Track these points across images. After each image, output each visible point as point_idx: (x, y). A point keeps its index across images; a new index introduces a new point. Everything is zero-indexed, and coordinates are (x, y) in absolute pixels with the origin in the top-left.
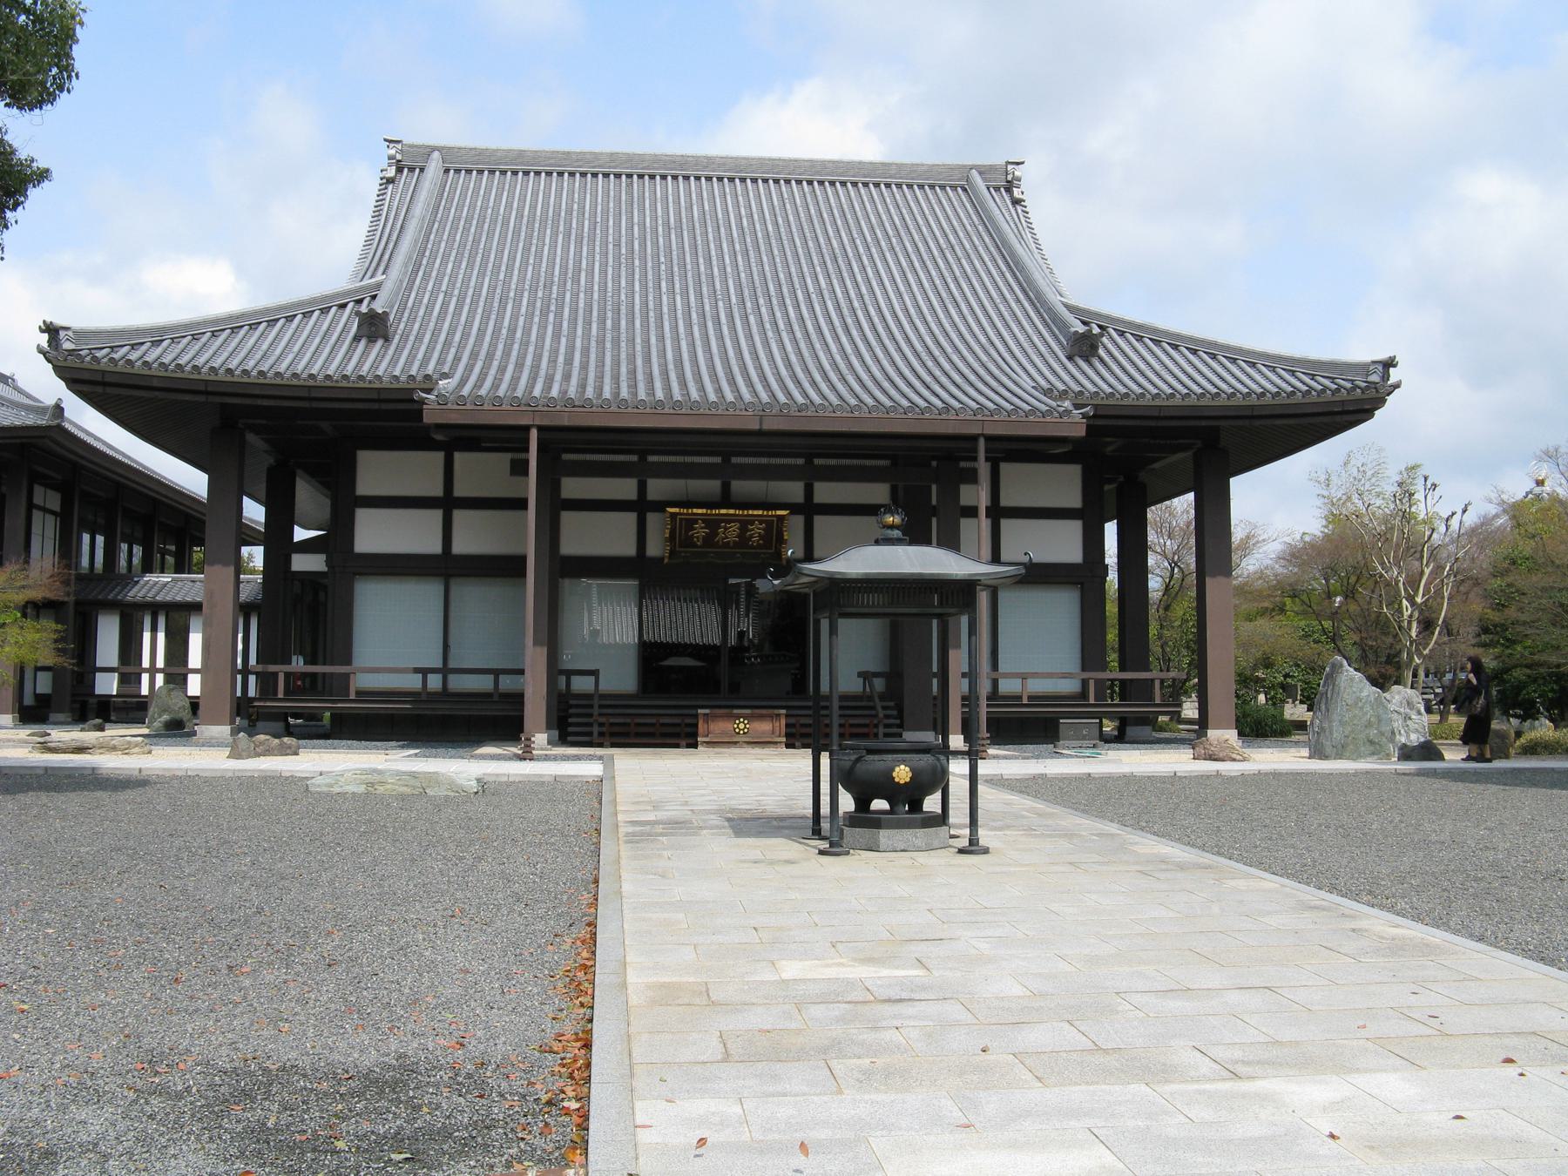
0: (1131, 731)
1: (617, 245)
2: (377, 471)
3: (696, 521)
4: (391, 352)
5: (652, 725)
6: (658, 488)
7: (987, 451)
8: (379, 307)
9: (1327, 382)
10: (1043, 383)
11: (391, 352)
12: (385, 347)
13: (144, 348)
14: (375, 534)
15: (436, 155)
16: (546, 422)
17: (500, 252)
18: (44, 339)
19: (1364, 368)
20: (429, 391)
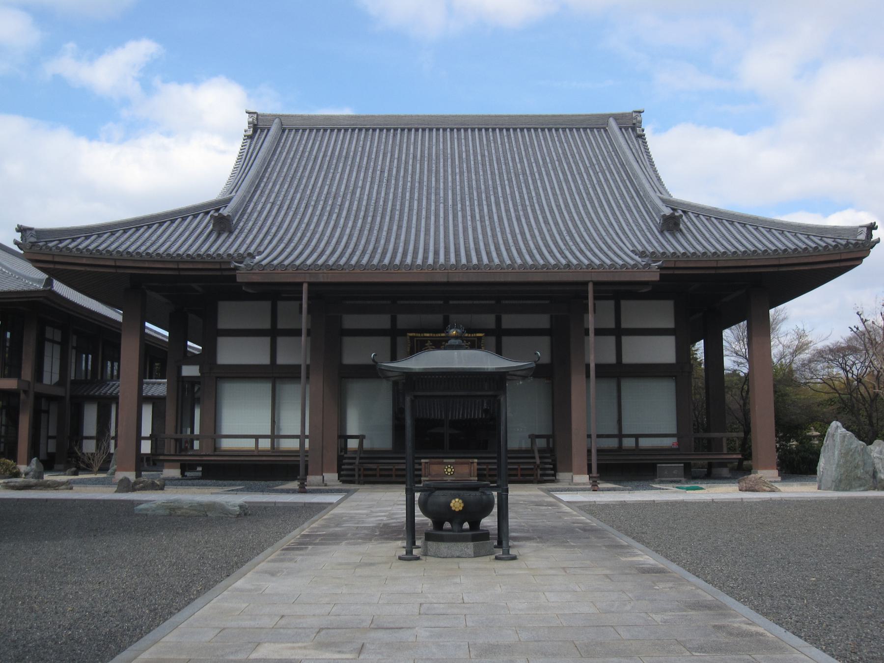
0: (715, 471)
1: (382, 172)
2: (229, 315)
3: (426, 341)
4: (231, 240)
5: (516, 469)
6: (404, 320)
7: (595, 292)
8: (225, 212)
9: (830, 241)
10: (640, 248)
11: (231, 240)
12: (229, 237)
13: (79, 241)
14: (230, 353)
15: (277, 121)
16: (313, 280)
17: (309, 178)
18: (18, 236)
19: (854, 230)
20: (241, 263)
